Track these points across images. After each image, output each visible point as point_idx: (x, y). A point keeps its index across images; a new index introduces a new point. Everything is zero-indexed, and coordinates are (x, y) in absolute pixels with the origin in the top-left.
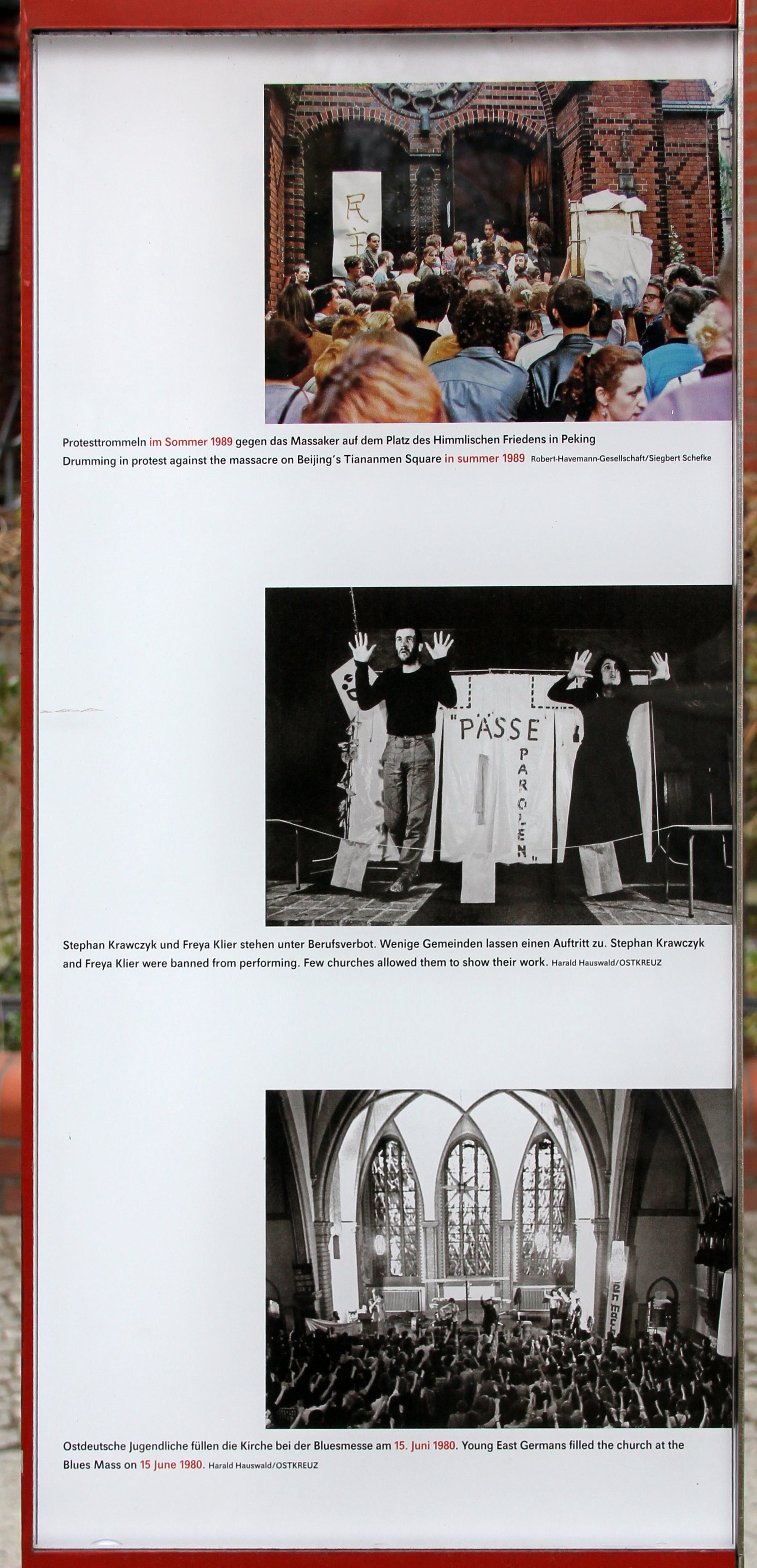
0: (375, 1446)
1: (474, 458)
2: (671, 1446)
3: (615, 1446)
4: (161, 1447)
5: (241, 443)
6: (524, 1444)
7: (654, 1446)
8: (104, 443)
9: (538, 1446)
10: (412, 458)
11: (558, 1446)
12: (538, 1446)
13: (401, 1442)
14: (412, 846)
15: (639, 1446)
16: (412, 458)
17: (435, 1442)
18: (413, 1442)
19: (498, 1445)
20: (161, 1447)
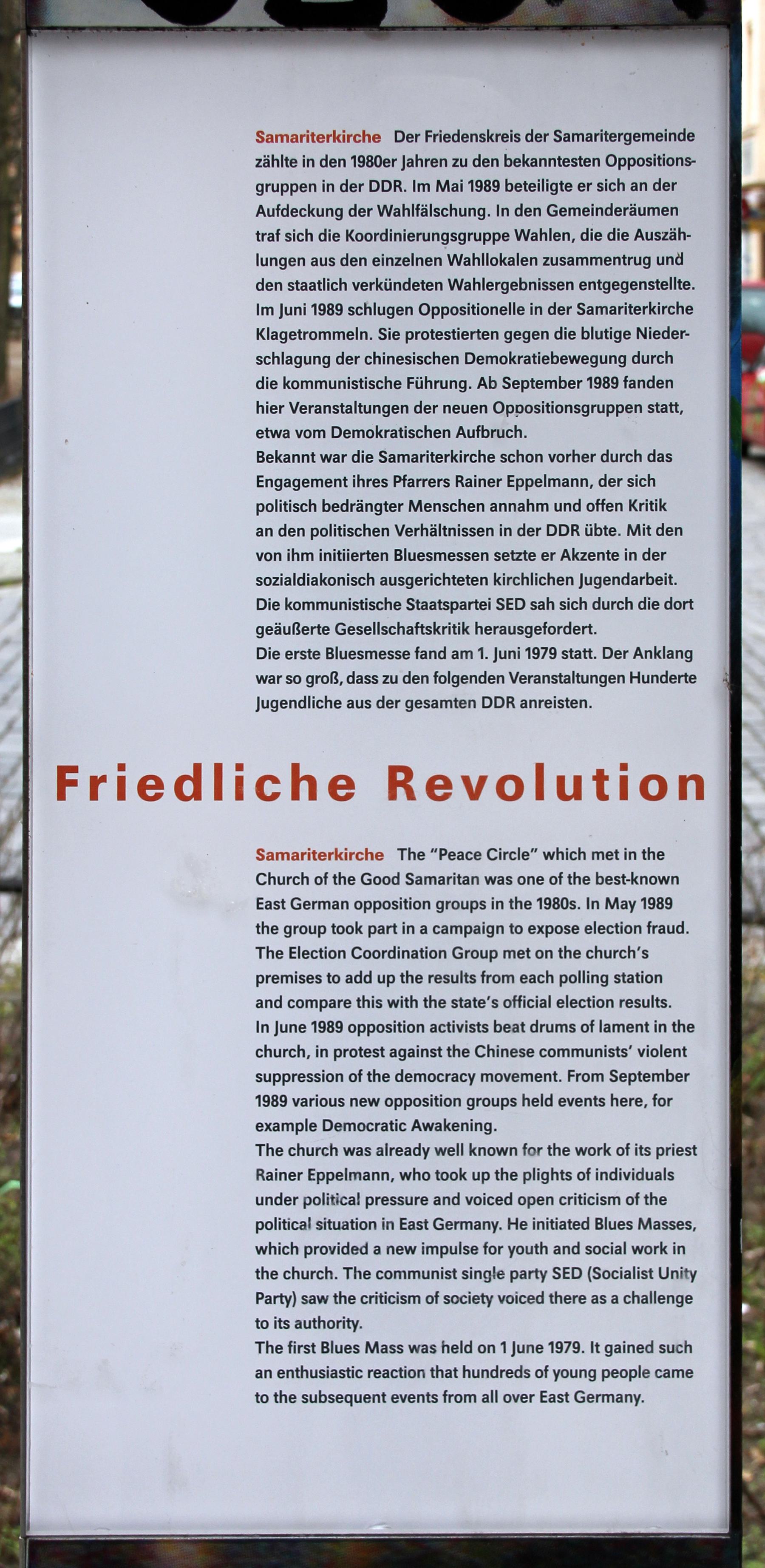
0: (344, 704)
1: (321, 383)
2: (514, 905)
3: (583, 955)
4: (302, 704)
5: (547, 1102)
6: (438, 1222)
7: (312, 880)
8: (307, 336)
9: (316, 905)
10: (601, 1273)
11: (546, 679)
12: (316, 905)
13: (321, 1229)
14: (450, 794)
15: (617, 954)
16: (601, 1273)
17: (471, 182)
18: (277, 1022)
19: (402, 1224)
20: (302, 704)
